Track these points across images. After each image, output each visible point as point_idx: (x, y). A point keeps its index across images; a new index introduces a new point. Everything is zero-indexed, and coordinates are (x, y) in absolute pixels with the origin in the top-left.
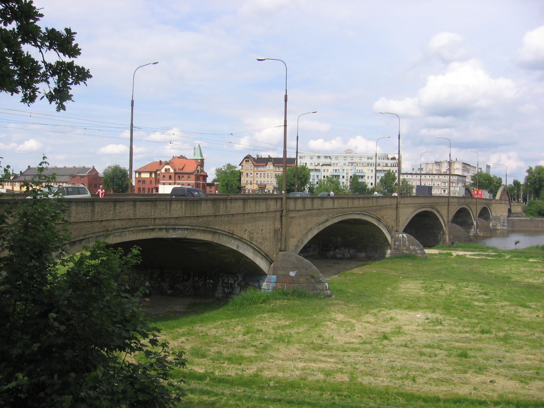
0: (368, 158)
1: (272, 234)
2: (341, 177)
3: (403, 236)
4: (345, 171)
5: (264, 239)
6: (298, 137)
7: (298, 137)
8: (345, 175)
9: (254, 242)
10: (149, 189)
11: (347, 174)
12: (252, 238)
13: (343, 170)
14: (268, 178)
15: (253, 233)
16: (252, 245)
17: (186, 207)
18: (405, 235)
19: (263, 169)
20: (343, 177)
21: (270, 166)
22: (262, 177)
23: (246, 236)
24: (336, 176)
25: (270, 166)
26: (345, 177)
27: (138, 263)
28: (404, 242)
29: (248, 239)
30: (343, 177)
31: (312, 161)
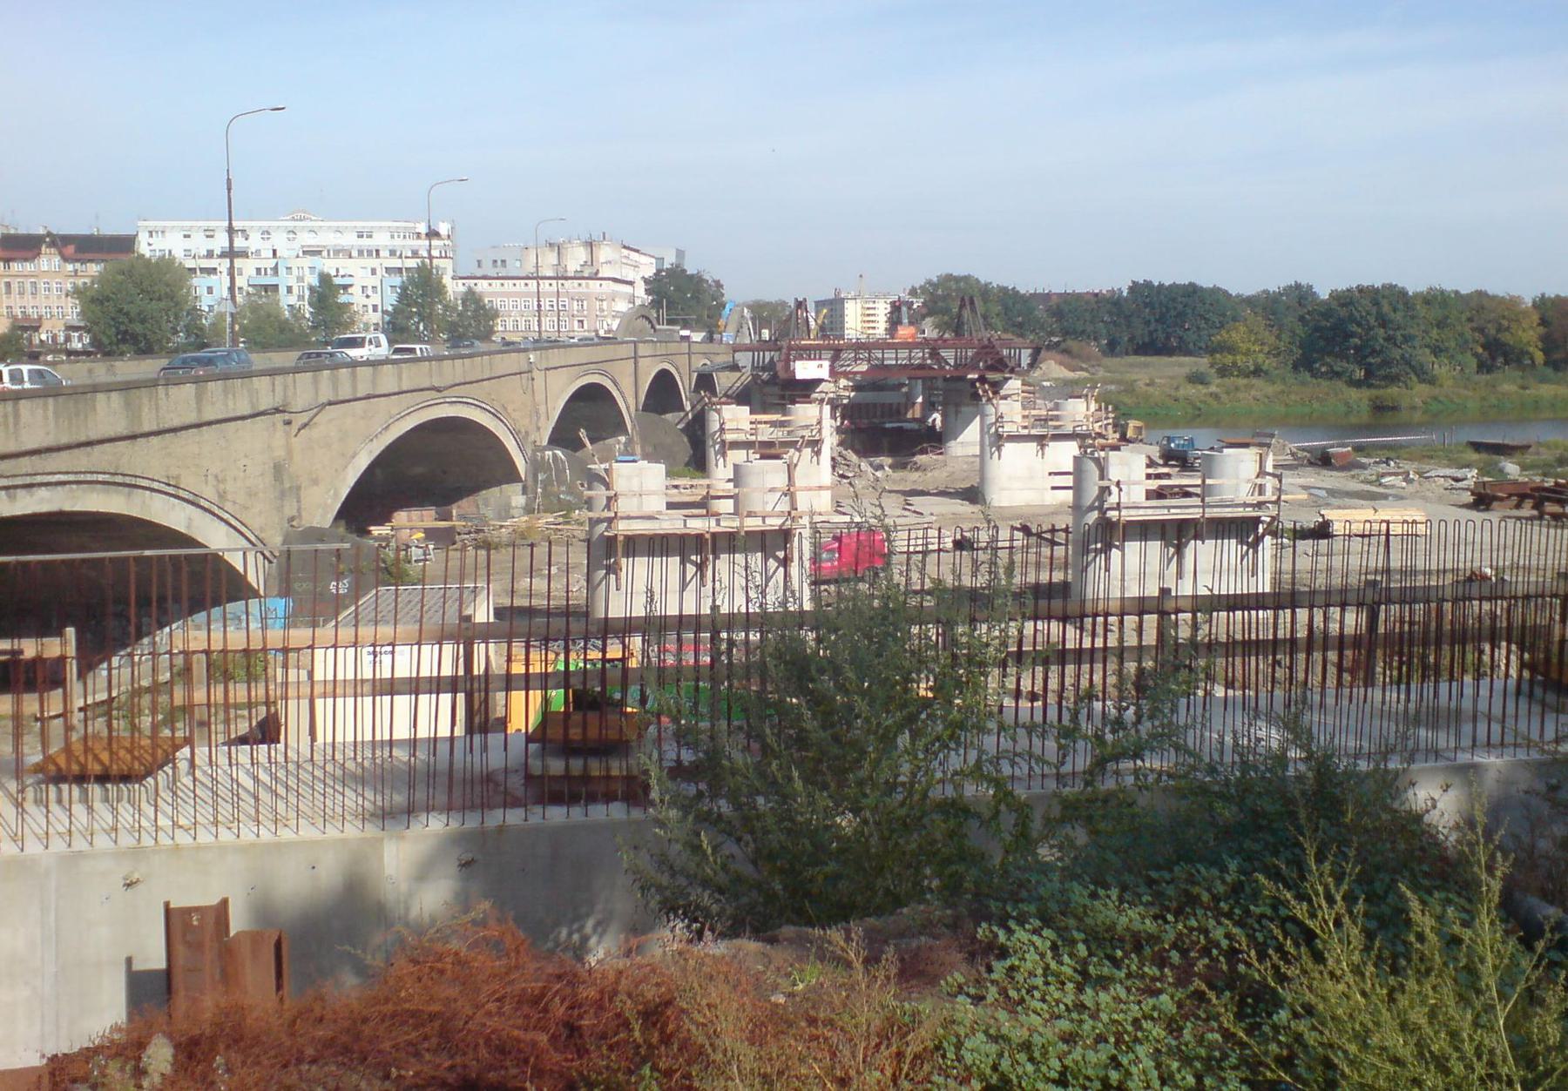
0: (361, 236)
1: (269, 478)
2: (283, 290)
3: (555, 456)
4: (295, 271)
5: (251, 494)
6: (229, 180)
7: (229, 180)
8: (292, 282)
9: (228, 506)
10: (1149, 476)
11: (300, 279)
12: (222, 495)
13: (289, 268)
14: (21, 293)
15: (224, 481)
16: (226, 516)
17: (57, 415)
18: (559, 453)
19: (29, 267)
20: (289, 290)
21: (48, 261)
22: (28, 296)
23: (209, 492)
24: (266, 288)
25: (48, 261)
26: (295, 290)
27: (1281, 759)
28: (560, 472)
29: (215, 499)
30: (289, 290)
31: (188, 244)
